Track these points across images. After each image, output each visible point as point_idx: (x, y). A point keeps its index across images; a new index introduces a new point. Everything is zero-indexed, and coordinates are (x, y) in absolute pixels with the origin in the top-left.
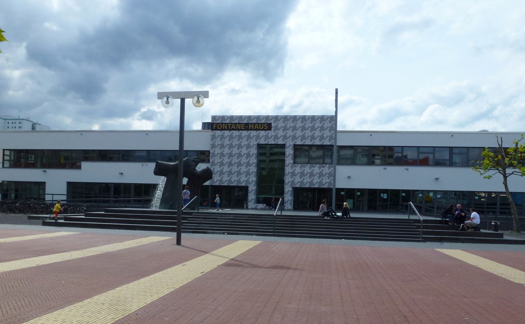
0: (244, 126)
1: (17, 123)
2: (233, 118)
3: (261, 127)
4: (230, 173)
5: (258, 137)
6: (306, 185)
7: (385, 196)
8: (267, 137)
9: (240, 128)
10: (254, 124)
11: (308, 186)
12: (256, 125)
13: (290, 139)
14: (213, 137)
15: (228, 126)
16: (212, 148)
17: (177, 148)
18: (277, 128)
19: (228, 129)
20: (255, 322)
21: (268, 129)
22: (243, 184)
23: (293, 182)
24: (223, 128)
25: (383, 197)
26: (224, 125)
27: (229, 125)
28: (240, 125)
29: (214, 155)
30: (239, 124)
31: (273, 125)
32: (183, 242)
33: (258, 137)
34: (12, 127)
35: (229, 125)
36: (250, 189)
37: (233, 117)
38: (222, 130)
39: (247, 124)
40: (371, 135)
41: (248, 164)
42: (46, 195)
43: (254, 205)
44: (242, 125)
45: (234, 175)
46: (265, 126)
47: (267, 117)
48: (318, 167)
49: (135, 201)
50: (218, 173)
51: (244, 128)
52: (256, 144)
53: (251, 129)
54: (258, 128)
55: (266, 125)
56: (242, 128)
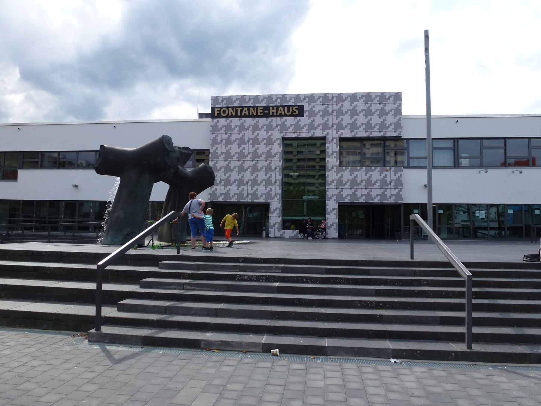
4: (241, 183)
15: (237, 111)
19: (236, 116)
27: (239, 109)
31: (306, 108)
38: (227, 117)
40: (457, 121)
43: (279, 232)
52: (281, 137)
53: (273, 116)
55: (296, 109)
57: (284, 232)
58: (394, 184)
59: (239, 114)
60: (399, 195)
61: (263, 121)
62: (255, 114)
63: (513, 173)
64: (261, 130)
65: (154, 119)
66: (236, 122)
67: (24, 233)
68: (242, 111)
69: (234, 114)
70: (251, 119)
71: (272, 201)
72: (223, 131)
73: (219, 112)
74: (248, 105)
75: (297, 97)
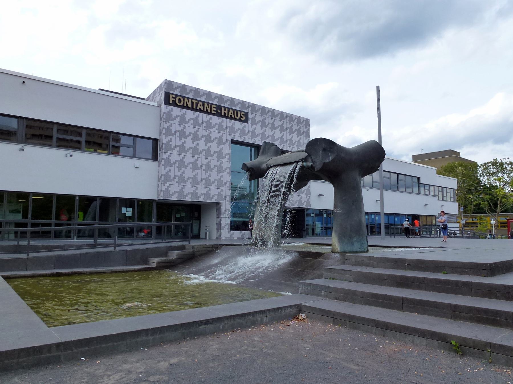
4: (195, 181)
5: (232, 131)
7: (127, 211)
15: (192, 103)
19: (192, 109)
21: (244, 120)
22: (214, 200)
25: (125, 214)
26: (186, 100)
27: (195, 102)
29: (169, 147)
31: (250, 116)
37: (199, 90)
38: (183, 107)
40: (24, 82)
43: (229, 233)
45: (173, 181)
48: (191, 168)
49: (32, 233)
51: (215, 113)
52: (230, 139)
53: (225, 116)
55: (243, 114)
57: (233, 233)
58: (204, 183)
59: (195, 107)
60: (308, 202)
61: (215, 120)
62: (209, 111)
63: (66, 156)
64: (188, 123)
65: (34, 75)
66: (190, 114)
67: (30, 244)
68: (197, 104)
69: (190, 106)
70: (205, 115)
71: (223, 202)
72: (215, 129)
73: (174, 100)
74: (225, 106)
75: (243, 103)
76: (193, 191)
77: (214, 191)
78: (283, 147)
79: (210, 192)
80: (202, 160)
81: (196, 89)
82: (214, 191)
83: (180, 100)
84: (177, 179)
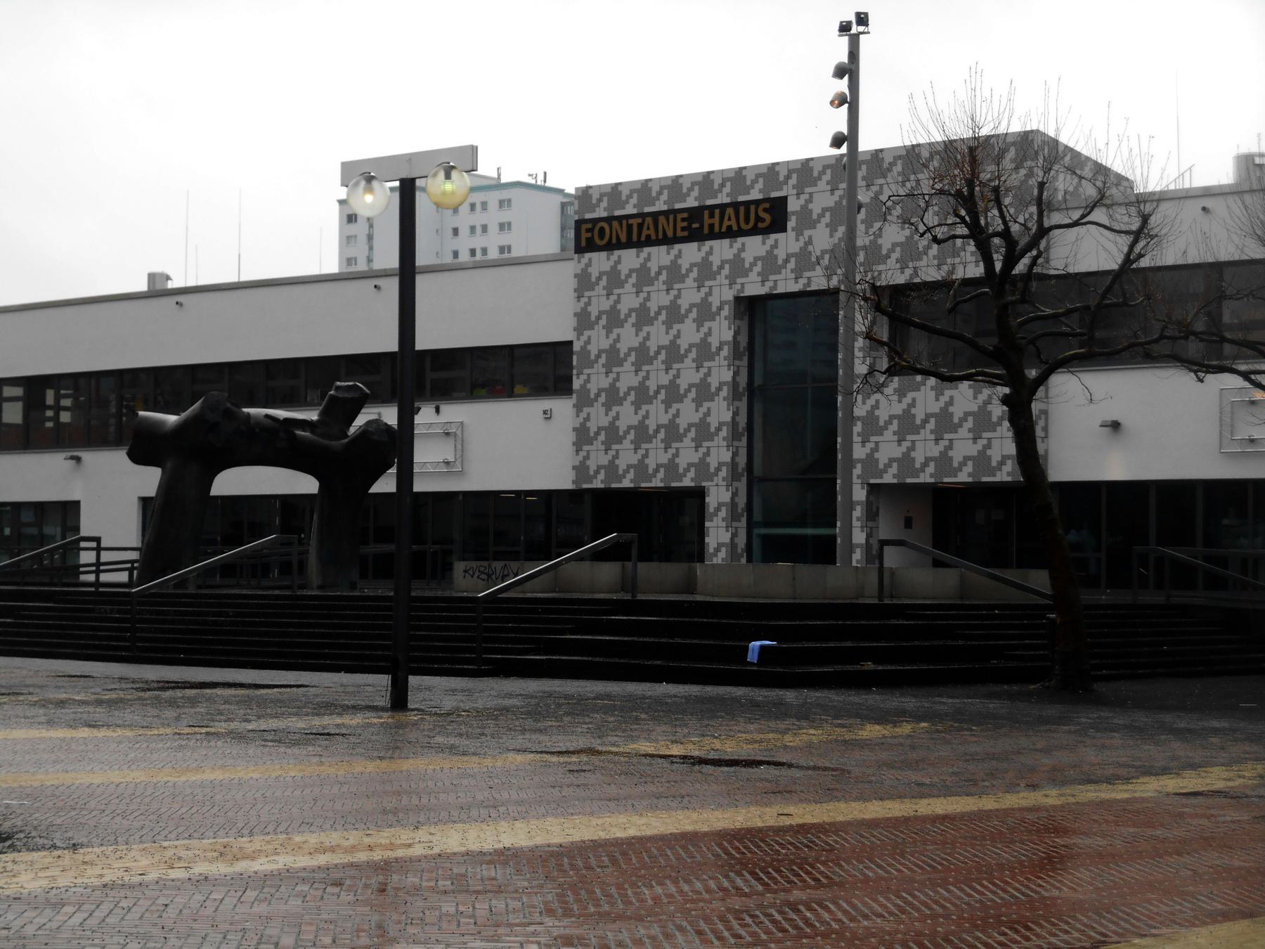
0: (685, 224)
1: (492, 206)
2: (919, 156)
3: (747, 220)
4: (642, 434)
5: (738, 268)
6: (922, 475)
8: (770, 265)
9: (670, 234)
10: (723, 207)
11: (969, 475)
12: (730, 211)
13: (788, 270)
14: (584, 283)
15: (630, 227)
16: (579, 330)
17: (390, 343)
18: (808, 221)
19: (629, 245)
20: (73, 885)
22: (687, 482)
23: (870, 461)
24: (614, 241)
26: (615, 224)
28: (671, 217)
30: (609, 220)
31: (793, 205)
32: (414, 701)
33: (738, 268)
34: (473, 229)
35: (632, 224)
36: (712, 501)
39: (694, 214)
41: (704, 393)
42: (140, 545)
44: (679, 216)
45: (922, 431)
46: (762, 214)
47: (771, 172)
50: (932, 425)
51: (686, 234)
52: (731, 298)
54: (735, 228)
55: (765, 210)
56: (680, 234)
68: (640, 226)
71: (710, 483)
76: (976, 454)
77: (688, 455)
78: (916, 273)
79: (951, 453)
80: (628, 379)
81: (872, 155)
82: (688, 455)
83: (602, 230)
84: (932, 425)
